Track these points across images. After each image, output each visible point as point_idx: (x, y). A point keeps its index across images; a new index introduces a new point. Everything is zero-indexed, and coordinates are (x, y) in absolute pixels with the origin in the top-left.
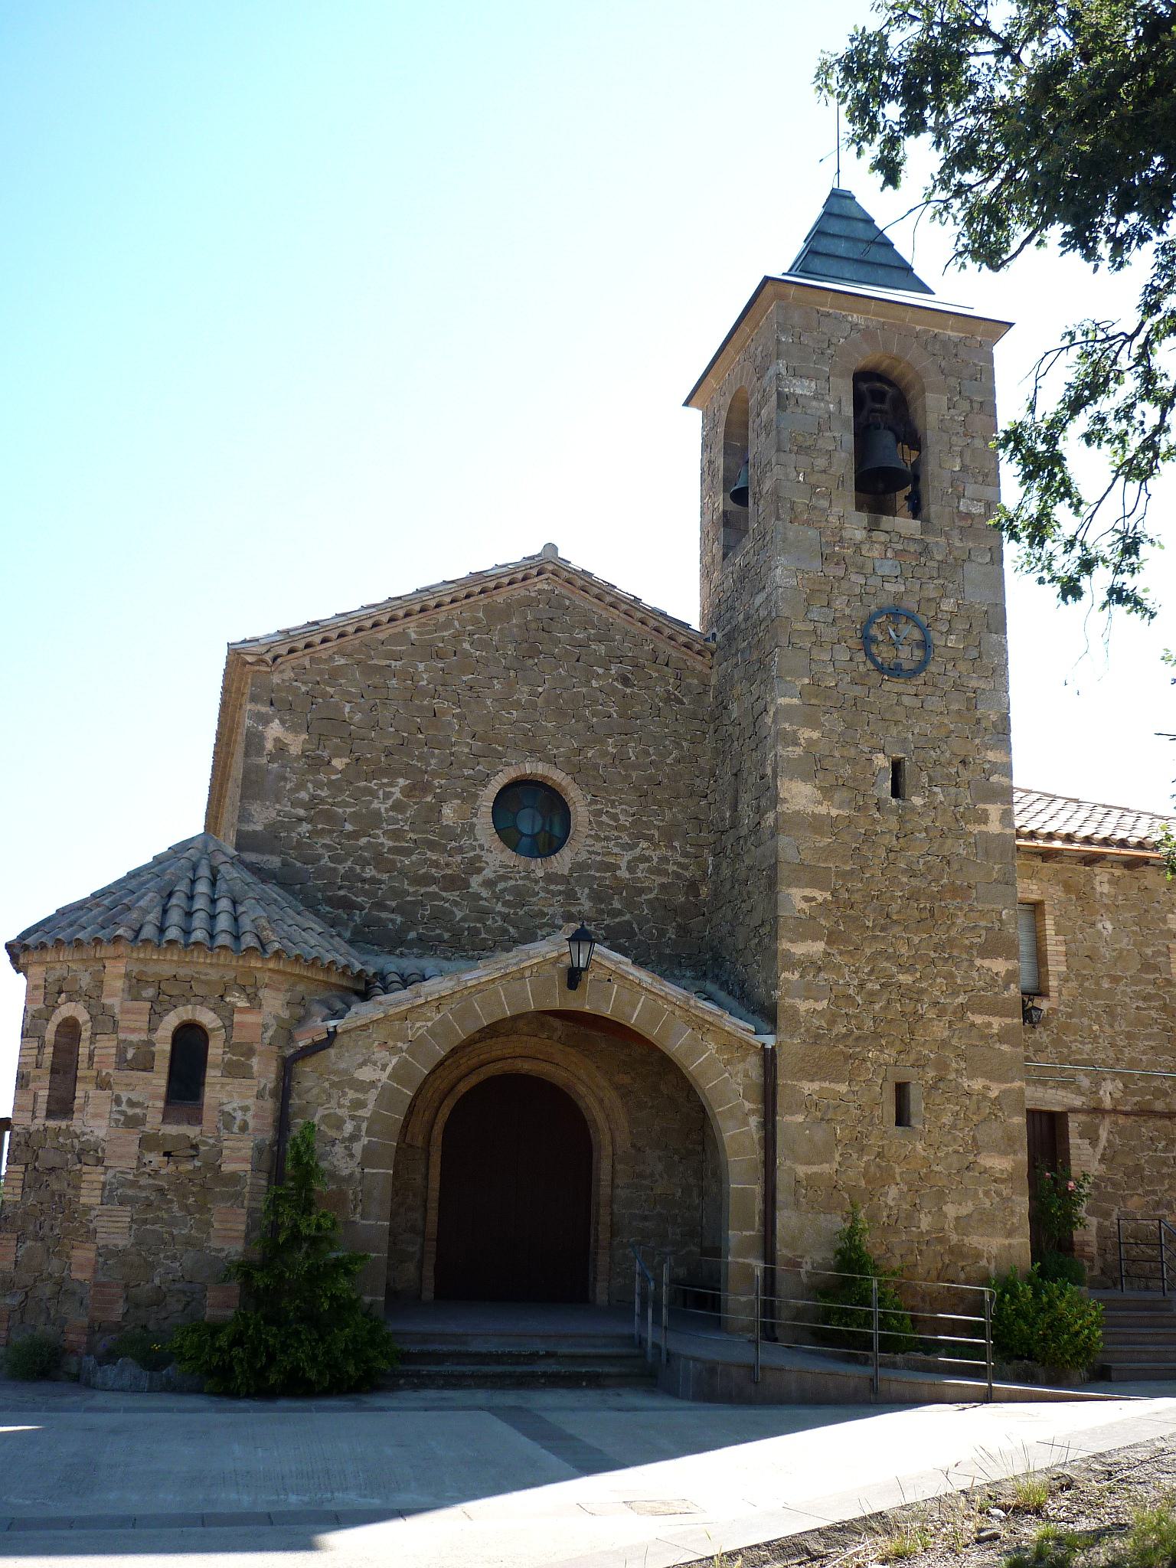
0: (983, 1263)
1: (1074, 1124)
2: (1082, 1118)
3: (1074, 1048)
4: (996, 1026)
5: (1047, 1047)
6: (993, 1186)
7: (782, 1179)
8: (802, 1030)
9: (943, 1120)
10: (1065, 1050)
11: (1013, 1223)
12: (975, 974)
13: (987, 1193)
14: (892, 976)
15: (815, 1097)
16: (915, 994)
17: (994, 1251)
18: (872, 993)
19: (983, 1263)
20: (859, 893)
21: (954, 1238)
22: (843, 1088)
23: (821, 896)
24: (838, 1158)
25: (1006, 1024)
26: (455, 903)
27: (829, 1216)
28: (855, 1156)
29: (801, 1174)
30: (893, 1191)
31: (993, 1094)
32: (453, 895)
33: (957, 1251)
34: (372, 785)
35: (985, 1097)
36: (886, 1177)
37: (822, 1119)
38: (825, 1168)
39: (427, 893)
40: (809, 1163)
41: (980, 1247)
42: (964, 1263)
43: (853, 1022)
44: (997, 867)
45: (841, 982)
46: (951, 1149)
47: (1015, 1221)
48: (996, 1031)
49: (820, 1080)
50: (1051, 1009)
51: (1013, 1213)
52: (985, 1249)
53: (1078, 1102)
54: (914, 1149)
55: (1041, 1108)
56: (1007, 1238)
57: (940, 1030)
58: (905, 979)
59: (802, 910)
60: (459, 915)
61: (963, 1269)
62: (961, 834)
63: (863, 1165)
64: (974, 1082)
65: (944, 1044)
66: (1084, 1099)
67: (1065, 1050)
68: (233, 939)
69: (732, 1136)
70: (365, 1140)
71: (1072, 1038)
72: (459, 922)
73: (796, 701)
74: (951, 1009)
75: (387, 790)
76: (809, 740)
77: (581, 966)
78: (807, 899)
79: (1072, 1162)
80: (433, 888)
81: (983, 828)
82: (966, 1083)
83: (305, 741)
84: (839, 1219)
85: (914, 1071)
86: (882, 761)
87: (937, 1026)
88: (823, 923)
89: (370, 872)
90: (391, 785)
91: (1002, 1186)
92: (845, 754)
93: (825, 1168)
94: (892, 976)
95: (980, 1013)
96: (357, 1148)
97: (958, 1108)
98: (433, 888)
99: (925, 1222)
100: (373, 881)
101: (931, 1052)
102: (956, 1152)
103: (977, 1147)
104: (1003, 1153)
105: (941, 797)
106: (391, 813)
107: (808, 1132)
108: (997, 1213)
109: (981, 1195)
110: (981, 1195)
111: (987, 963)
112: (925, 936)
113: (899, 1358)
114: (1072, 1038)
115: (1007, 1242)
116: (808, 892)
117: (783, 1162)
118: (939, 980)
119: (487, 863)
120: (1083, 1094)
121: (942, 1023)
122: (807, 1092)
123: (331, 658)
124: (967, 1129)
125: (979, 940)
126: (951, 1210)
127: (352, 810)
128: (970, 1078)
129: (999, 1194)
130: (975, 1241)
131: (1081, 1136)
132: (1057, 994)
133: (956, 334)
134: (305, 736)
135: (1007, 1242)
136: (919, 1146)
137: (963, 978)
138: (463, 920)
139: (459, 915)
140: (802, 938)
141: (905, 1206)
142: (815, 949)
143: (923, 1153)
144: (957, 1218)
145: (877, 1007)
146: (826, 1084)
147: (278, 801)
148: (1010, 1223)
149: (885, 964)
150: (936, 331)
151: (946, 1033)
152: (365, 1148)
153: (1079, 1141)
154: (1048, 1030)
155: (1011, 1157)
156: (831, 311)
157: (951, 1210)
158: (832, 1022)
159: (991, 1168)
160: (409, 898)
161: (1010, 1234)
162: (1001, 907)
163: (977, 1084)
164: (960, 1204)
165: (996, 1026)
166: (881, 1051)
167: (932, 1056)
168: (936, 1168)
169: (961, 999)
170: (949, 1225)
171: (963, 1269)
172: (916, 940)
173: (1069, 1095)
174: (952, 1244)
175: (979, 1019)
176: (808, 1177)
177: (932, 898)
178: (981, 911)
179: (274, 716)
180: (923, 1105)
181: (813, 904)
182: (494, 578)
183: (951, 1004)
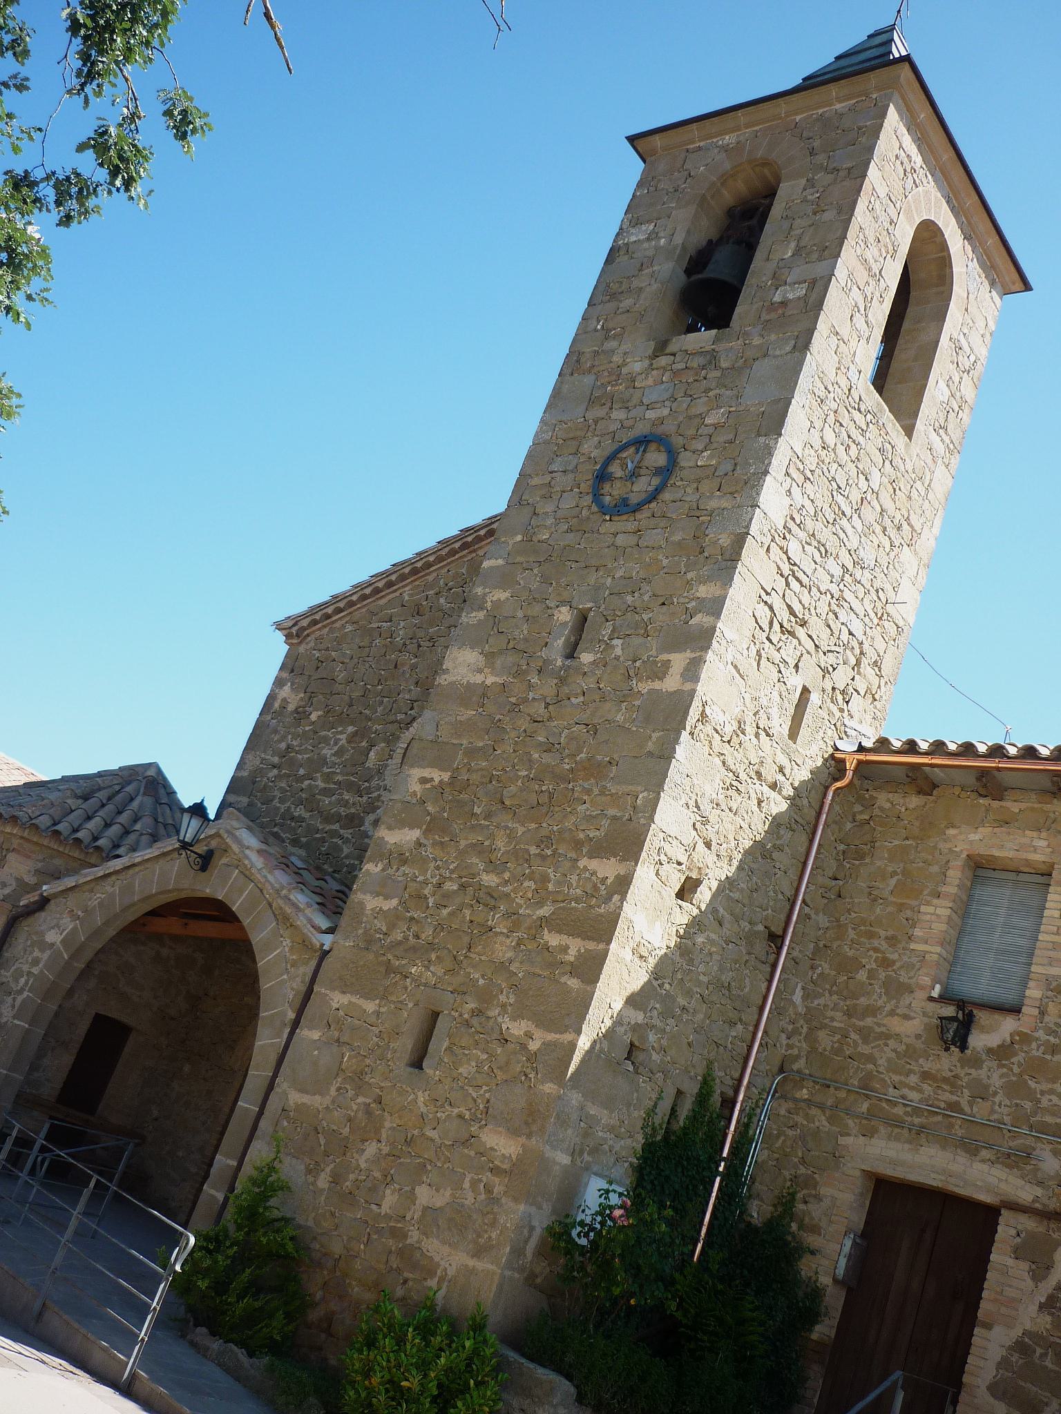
0: (432, 1283)
1: (1007, 1229)
2: (1028, 1224)
3: (1045, 1102)
4: (573, 952)
5: (995, 1094)
6: (487, 1177)
7: (273, 1104)
8: (360, 932)
9: (461, 1070)
10: (1028, 1105)
11: (490, 1237)
12: (574, 879)
13: (474, 1184)
14: (473, 876)
15: (341, 1013)
16: (489, 899)
17: (451, 1272)
18: (447, 896)
19: (432, 1283)
20: (480, 773)
21: (414, 1236)
22: (370, 1006)
23: (438, 776)
24: (333, 1092)
25: (586, 949)
26: (347, 841)
27: (294, 1161)
28: (351, 1093)
29: (291, 1103)
30: (371, 1149)
31: (534, 1046)
32: (347, 833)
33: (409, 1255)
34: (329, 733)
35: (524, 1046)
36: (368, 1128)
37: (338, 1041)
38: (317, 1101)
39: (331, 830)
40: (303, 1091)
41: (437, 1259)
42: (411, 1276)
43: (414, 928)
44: (655, 735)
45: (421, 878)
46: (456, 1111)
47: (494, 1235)
48: (572, 959)
49: (352, 993)
50: (1020, 1034)
51: (493, 1224)
52: (442, 1263)
53: (1026, 1193)
54: (415, 1101)
55: (957, 1190)
56: (473, 1257)
57: (503, 949)
58: (489, 879)
59: (415, 793)
60: (346, 850)
61: (406, 1281)
62: (626, 696)
63: (355, 1107)
64: (516, 1024)
65: (503, 967)
66: (1039, 1192)
67: (1028, 1105)
68: (91, 838)
69: (262, 1046)
70: (26, 994)
71: (1046, 1086)
72: (343, 858)
73: (500, 562)
74: (528, 922)
75: (338, 737)
76: (498, 604)
77: (186, 840)
78: (424, 781)
79: (985, 1294)
80: (336, 826)
81: (657, 685)
82: (506, 1023)
83: (302, 699)
84: (303, 1167)
85: (449, 997)
86: (564, 615)
87: (501, 944)
88: (430, 808)
89: (299, 812)
90: (341, 732)
91: (497, 1180)
92: (529, 613)
93: (317, 1101)
94: (473, 876)
95: (560, 932)
96: (20, 999)
97: (485, 1056)
98: (336, 826)
99: (389, 1200)
100: (301, 819)
101: (483, 976)
102: (460, 1116)
103: (486, 1114)
104: (514, 1132)
105: (618, 651)
106: (333, 758)
107: (316, 1052)
108: (475, 1216)
109: (467, 1185)
110: (467, 1185)
111: (593, 864)
112: (533, 826)
113: (216, 1345)
114: (1046, 1086)
115: (471, 1263)
116: (426, 773)
117: (282, 1084)
118: (526, 884)
119: (383, 802)
120: (1040, 1183)
121: (508, 941)
122: (335, 1006)
123: (343, 626)
124: (485, 1088)
125: (598, 833)
126: (424, 1195)
127: (308, 756)
128: (514, 1019)
129: (488, 1190)
130: (434, 1248)
131: (1018, 1253)
132: (1036, 1012)
133: (843, 105)
134: (302, 695)
135: (471, 1263)
136: (422, 1097)
137: (559, 883)
138: (347, 857)
139: (346, 850)
140: (402, 824)
141: (377, 1174)
142: (408, 838)
143: (423, 1109)
144: (426, 1209)
145: (445, 912)
146: (354, 999)
147: (265, 752)
148: (486, 1236)
149: (475, 860)
150: (820, 111)
151: (510, 954)
152: (24, 1001)
153: (1010, 1262)
154: (1004, 1066)
155: (523, 1139)
156: (702, 144)
157: (424, 1195)
158: (392, 926)
159: (492, 1149)
160: (318, 836)
161: (478, 1253)
162: (639, 788)
163: (517, 1028)
164: (437, 1190)
165: (573, 952)
166: (427, 968)
167: (481, 982)
168: (430, 1133)
169: (545, 911)
170: (415, 1213)
171: (406, 1281)
172: (521, 830)
173: (1011, 1179)
174: (409, 1241)
175: (553, 940)
176: (300, 1108)
177: (560, 778)
178: (612, 795)
179: (289, 680)
180: (446, 1044)
181: (428, 786)
182: (472, 531)
183: (529, 916)
